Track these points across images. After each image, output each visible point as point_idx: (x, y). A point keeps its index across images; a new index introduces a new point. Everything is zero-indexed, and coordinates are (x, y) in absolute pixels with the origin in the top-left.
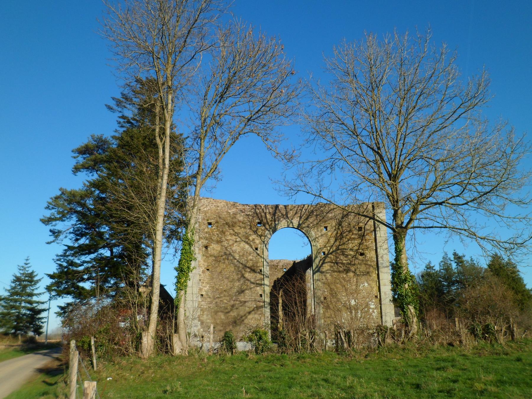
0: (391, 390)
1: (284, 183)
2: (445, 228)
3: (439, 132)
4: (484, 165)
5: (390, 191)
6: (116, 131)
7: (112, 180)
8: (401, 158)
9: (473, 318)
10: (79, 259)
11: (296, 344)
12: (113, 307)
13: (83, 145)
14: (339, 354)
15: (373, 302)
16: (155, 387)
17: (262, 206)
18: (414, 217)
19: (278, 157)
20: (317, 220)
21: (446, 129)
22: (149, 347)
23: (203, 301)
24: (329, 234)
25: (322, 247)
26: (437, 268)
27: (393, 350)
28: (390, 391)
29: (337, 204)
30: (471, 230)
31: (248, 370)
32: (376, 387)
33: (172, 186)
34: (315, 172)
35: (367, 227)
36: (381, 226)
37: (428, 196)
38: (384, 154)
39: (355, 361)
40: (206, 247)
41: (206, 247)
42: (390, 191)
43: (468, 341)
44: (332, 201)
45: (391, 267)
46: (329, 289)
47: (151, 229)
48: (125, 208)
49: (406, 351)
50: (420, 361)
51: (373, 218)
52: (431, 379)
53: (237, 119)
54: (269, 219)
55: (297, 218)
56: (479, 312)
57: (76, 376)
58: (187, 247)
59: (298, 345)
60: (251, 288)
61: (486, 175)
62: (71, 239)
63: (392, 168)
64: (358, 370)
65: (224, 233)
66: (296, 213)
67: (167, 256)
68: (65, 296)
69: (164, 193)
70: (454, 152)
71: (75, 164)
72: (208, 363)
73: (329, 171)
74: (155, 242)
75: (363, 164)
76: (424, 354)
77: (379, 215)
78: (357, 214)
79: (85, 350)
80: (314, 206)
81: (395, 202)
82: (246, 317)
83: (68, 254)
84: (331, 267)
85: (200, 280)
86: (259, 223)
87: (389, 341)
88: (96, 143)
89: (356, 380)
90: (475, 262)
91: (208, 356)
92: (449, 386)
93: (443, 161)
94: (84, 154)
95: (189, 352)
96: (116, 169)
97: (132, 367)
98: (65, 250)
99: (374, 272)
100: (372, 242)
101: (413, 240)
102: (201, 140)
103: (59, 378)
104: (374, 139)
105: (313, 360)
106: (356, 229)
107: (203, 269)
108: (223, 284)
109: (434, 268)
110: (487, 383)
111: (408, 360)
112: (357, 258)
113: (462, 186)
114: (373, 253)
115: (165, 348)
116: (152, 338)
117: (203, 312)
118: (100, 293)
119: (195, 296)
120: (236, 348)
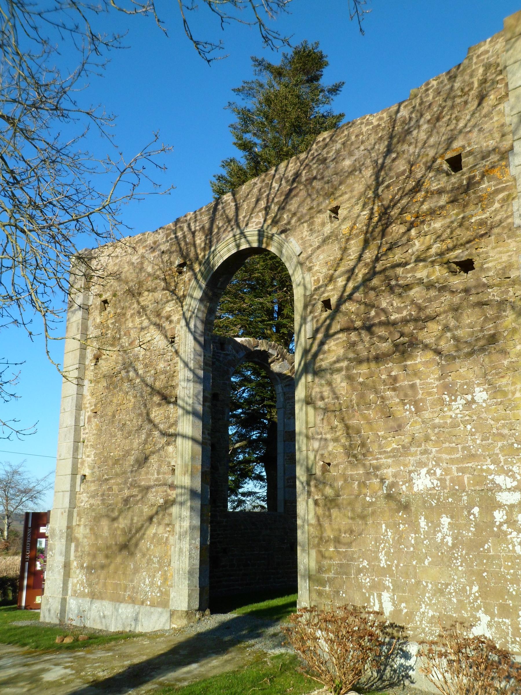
54: (200, 245)
106: (439, 171)
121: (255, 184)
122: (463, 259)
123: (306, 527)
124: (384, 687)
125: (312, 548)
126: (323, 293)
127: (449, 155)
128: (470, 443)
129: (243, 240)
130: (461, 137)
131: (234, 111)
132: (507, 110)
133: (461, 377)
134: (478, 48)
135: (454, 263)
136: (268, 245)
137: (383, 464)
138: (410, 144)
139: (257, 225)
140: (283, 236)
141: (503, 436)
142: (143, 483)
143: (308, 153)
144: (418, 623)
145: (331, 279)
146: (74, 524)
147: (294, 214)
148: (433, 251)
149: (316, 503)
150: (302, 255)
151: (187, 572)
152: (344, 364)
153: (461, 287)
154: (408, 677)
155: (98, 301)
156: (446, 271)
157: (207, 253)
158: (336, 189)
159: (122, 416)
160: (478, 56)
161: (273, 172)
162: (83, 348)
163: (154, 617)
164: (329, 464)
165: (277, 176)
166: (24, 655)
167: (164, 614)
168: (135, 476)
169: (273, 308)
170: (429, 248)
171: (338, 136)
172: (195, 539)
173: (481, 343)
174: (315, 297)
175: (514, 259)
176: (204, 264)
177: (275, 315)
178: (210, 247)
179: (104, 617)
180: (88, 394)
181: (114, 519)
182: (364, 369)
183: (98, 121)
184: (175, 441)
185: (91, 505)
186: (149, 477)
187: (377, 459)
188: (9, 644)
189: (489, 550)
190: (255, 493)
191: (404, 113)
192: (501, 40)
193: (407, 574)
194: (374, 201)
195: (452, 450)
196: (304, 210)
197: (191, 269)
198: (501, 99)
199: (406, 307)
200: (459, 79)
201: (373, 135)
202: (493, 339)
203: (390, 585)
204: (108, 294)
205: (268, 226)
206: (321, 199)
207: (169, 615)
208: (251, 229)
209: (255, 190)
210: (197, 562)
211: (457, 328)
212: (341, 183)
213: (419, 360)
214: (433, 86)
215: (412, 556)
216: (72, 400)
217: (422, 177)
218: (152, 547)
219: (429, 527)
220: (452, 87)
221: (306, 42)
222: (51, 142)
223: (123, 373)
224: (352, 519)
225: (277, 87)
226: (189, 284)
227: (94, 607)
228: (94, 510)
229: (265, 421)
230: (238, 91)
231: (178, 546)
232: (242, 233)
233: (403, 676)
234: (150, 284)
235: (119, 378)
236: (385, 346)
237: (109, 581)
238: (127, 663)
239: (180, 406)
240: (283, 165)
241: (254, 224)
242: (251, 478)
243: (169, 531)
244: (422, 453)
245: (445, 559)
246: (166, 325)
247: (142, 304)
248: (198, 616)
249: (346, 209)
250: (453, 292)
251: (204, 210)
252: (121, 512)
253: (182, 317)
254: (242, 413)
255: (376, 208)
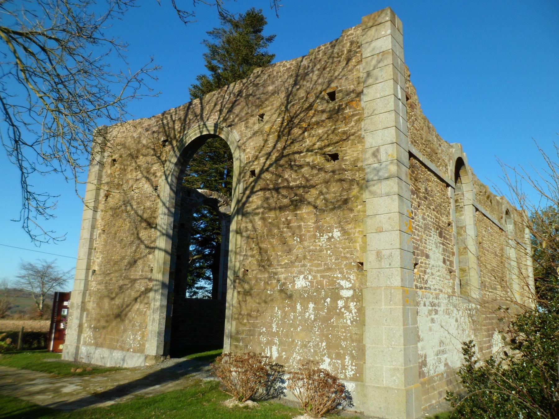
54: (178, 129)
121: (214, 94)
122: (333, 153)
123: (231, 308)
124: (269, 399)
125: (234, 320)
126: (251, 166)
127: (329, 91)
128: (329, 261)
129: (205, 129)
130: (336, 81)
131: (206, 45)
132: (361, 69)
133: (326, 222)
134: (348, 32)
135: (328, 154)
136: (220, 133)
137: (279, 272)
138: (308, 81)
139: (214, 120)
140: (229, 128)
141: (346, 258)
142: (132, 277)
143: (248, 80)
144: (291, 363)
145: (257, 158)
146: (86, 300)
147: (237, 116)
148: (316, 146)
149: (239, 293)
150: (240, 142)
151: (157, 332)
152: (261, 210)
153: (331, 169)
154: (283, 393)
155: (110, 160)
156: (323, 159)
157: (182, 135)
158: (263, 103)
159: (122, 235)
160: (348, 36)
161: (226, 88)
162: (98, 189)
163: (135, 359)
164: (248, 271)
165: (228, 92)
166: (50, 378)
167: (141, 357)
168: (127, 273)
169: (224, 171)
170: (314, 144)
171: (266, 71)
172: (163, 313)
173: (339, 203)
174: (246, 168)
175: (360, 155)
176: (179, 141)
177: (225, 177)
178: (184, 131)
179: (103, 358)
180: (100, 219)
181: (113, 299)
182: (272, 214)
183: (117, 47)
184: (154, 252)
185: (98, 289)
186: (136, 273)
187: (276, 269)
188: (41, 371)
189: (333, 322)
190: (205, 288)
191: (305, 62)
192: (360, 29)
193: (287, 335)
194: (285, 113)
195: (319, 265)
196: (243, 114)
197: (171, 143)
198: (359, 62)
199: (299, 178)
200: (336, 47)
201: (287, 73)
202: (346, 202)
203: (277, 342)
204: (117, 155)
205: (221, 122)
206: (254, 108)
207: (144, 358)
208: (210, 123)
209: (214, 99)
210: (163, 327)
211: (327, 193)
212: (266, 100)
213: (304, 211)
214: (322, 49)
215: (292, 325)
216: (89, 222)
217: (313, 102)
218: (136, 317)
219: (302, 309)
220: (333, 51)
221: (254, 8)
222: (86, 57)
223: (123, 208)
224: (259, 303)
225: (235, 34)
226: (169, 153)
227: (97, 352)
228: (100, 292)
229: (214, 243)
230: (210, 33)
231: (152, 317)
232: (204, 124)
233: (280, 393)
234: (144, 151)
235: (120, 210)
236: (286, 201)
237: (107, 336)
238: (116, 384)
239: (158, 230)
240: (232, 85)
241: (212, 119)
242: (203, 279)
243: (147, 307)
244: (301, 266)
245: (309, 327)
246: (152, 178)
247: (138, 164)
248: (162, 359)
249: (268, 116)
250: (326, 172)
251: (181, 108)
252: (117, 294)
253: (163, 174)
254: (199, 237)
255: (286, 117)
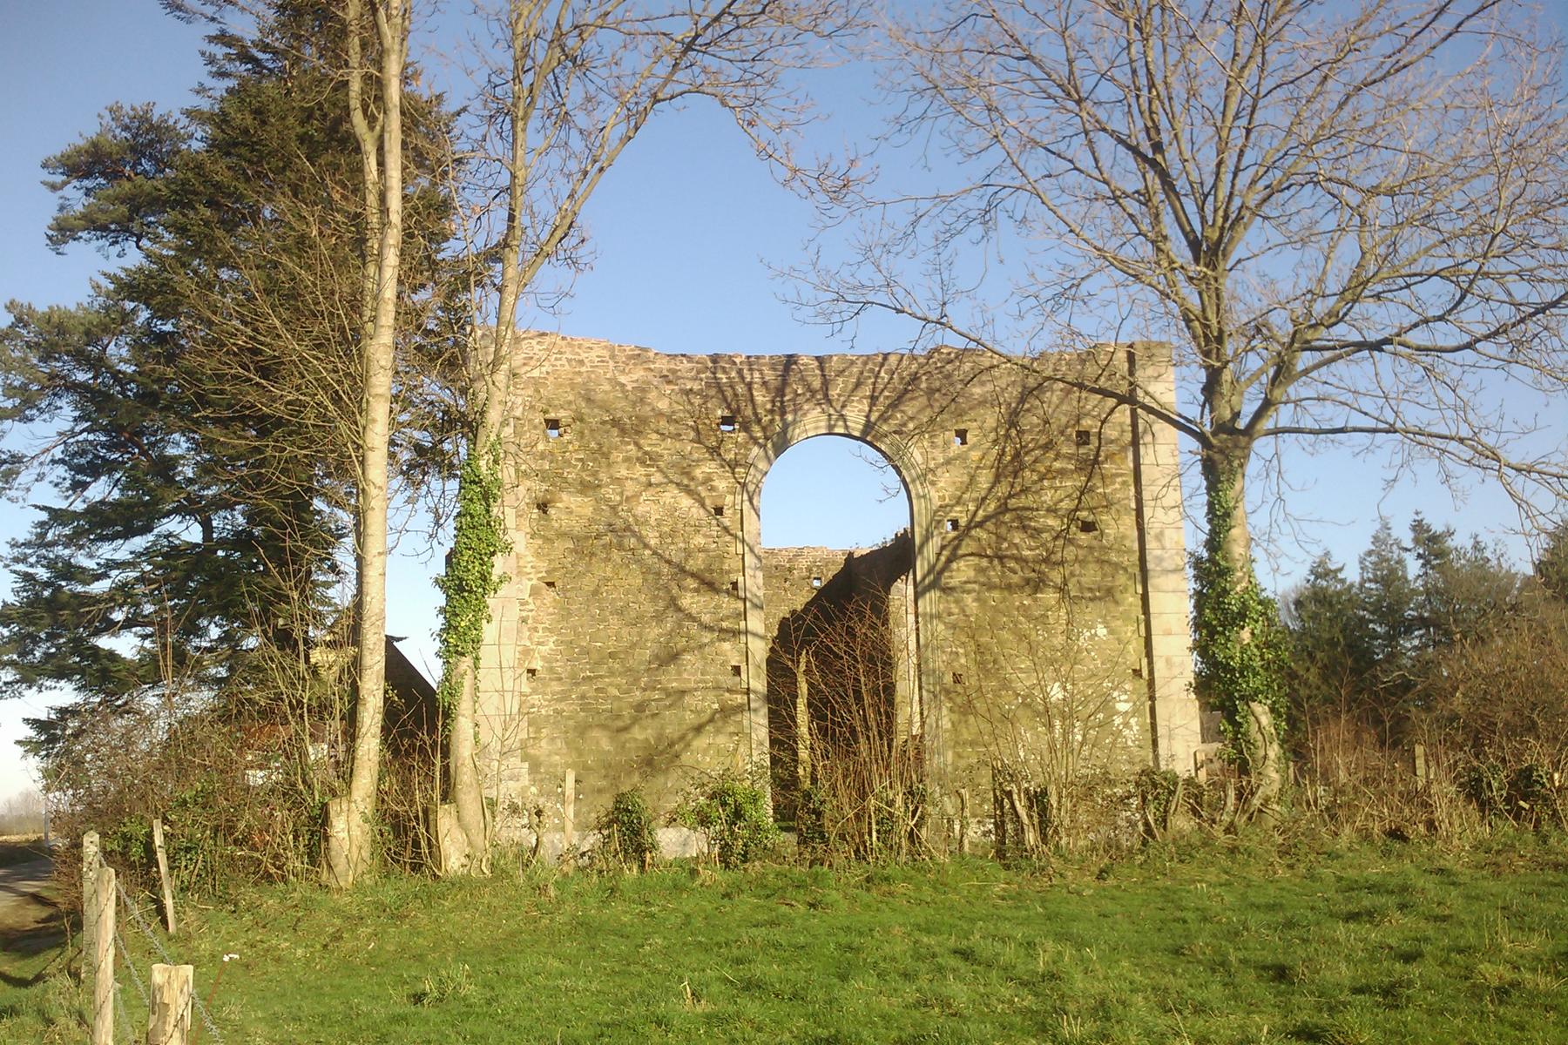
0: (1191, 986)
1: (812, 277)
2: (1387, 432)
3: (1381, 85)
4: (1540, 208)
5: (1194, 302)
6: (201, 90)
7: (195, 272)
8: (1237, 181)
9: (1478, 745)
10: (91, 556)
11: (861, 835)
12: (225, 717)
13: (81, 143)
14: (1007, 867)
15: (1126, 692)
16: (379, 985)
17: (738, 360)
18: (1277, 393)
19: (796, 184)
20: (932, 406)
21: (1408, 76)
22: (354, 849)
23: (534, 691)
24: (975, 455)
25: (947, 501)
26: (1352, 575)
27: (1194, 852)
28: (1186, 987)
29: (1004, 351)
30: (1483, 438)
31: (698, 922)
32: (1137, 977)
33: (415, 290)
34: (925, 233)
35: (1110, 432)
36: (1160, 427)
37: (1333, 320)
38: (1175, 170)
39: (1064, 891)
40: (543, 507)
41: (543, 507)
42: (1194, 302)
43: (1457, 823)
44: (986, 339)
45: (1191, 572)
46: (972, 647)
47: (345, 445)
48: (249, 370)
49: (1239, 856)
50: (1289, 891)
51: (1129, 399)
52: (1326, 948)
53: (646, 45)
54: (764, 404)
55: (860, 401)
56: (1500, 725)
57: (112, 952)
58: (478, 508)
59: (867, 837)
60: (701, 647)
61: (1548, 242)
62: (57, 485)
63: (1203, 220)
64: (1074, 918)
65: (606, 456)
66: (858, 385)
67: (405, 538)
68: (48, 683)
69: (387, 317)
70: (1433, 160)
71: (56, 214)
72: (561, 902)
73: (976, 230)
74: (363, 490)
75: (1099, 204)
76: (1301, 869)
77: (1156, 388)
78: (1074, 385)
79: (132, 866)
80: (922, 360)
81: (1210, 342)
82: (688, 745)
83: (50, 536)
84: (981, 570)
85: (524, 620)
86: (726, 421)
87: (1182, 822)
88: (129, 136)
89: (1069, 952)
90: (1487, 554)
91: (558, 876)
92: (1389, 974)
93: (1391, 193)
94: (88, 175)
95: (492, 864)
96: (207, 231)
97: (299, 920)
98: (41, 524)
99: (1131, 590)
100: (1124, 483)
101: (1274, 475)
102: (514, 122)
103: (50, 961)
104: (1141, 113)
105: (918, 889)
107: (534, 582)
108: (602, 634)
109: (1340, 576)
110: (1520, 962)
111: (1249, 886)
112: (1071, 542)
113: (1457, 284)
114: (1128, 523)
115: (409, 852)
116: (366, 821)
117: (538, 731)
118: (176, 673)
119: (508, 674)
120: (654, 847)
129: (840, 423)
